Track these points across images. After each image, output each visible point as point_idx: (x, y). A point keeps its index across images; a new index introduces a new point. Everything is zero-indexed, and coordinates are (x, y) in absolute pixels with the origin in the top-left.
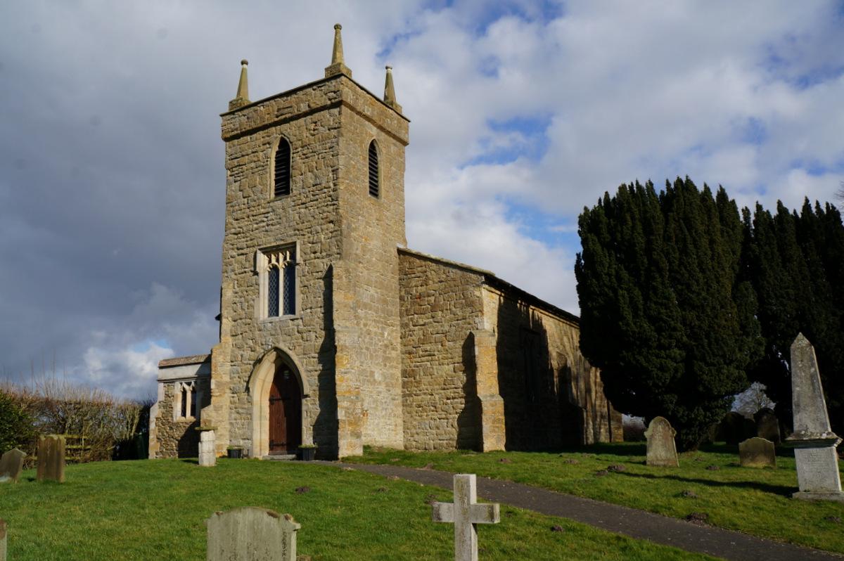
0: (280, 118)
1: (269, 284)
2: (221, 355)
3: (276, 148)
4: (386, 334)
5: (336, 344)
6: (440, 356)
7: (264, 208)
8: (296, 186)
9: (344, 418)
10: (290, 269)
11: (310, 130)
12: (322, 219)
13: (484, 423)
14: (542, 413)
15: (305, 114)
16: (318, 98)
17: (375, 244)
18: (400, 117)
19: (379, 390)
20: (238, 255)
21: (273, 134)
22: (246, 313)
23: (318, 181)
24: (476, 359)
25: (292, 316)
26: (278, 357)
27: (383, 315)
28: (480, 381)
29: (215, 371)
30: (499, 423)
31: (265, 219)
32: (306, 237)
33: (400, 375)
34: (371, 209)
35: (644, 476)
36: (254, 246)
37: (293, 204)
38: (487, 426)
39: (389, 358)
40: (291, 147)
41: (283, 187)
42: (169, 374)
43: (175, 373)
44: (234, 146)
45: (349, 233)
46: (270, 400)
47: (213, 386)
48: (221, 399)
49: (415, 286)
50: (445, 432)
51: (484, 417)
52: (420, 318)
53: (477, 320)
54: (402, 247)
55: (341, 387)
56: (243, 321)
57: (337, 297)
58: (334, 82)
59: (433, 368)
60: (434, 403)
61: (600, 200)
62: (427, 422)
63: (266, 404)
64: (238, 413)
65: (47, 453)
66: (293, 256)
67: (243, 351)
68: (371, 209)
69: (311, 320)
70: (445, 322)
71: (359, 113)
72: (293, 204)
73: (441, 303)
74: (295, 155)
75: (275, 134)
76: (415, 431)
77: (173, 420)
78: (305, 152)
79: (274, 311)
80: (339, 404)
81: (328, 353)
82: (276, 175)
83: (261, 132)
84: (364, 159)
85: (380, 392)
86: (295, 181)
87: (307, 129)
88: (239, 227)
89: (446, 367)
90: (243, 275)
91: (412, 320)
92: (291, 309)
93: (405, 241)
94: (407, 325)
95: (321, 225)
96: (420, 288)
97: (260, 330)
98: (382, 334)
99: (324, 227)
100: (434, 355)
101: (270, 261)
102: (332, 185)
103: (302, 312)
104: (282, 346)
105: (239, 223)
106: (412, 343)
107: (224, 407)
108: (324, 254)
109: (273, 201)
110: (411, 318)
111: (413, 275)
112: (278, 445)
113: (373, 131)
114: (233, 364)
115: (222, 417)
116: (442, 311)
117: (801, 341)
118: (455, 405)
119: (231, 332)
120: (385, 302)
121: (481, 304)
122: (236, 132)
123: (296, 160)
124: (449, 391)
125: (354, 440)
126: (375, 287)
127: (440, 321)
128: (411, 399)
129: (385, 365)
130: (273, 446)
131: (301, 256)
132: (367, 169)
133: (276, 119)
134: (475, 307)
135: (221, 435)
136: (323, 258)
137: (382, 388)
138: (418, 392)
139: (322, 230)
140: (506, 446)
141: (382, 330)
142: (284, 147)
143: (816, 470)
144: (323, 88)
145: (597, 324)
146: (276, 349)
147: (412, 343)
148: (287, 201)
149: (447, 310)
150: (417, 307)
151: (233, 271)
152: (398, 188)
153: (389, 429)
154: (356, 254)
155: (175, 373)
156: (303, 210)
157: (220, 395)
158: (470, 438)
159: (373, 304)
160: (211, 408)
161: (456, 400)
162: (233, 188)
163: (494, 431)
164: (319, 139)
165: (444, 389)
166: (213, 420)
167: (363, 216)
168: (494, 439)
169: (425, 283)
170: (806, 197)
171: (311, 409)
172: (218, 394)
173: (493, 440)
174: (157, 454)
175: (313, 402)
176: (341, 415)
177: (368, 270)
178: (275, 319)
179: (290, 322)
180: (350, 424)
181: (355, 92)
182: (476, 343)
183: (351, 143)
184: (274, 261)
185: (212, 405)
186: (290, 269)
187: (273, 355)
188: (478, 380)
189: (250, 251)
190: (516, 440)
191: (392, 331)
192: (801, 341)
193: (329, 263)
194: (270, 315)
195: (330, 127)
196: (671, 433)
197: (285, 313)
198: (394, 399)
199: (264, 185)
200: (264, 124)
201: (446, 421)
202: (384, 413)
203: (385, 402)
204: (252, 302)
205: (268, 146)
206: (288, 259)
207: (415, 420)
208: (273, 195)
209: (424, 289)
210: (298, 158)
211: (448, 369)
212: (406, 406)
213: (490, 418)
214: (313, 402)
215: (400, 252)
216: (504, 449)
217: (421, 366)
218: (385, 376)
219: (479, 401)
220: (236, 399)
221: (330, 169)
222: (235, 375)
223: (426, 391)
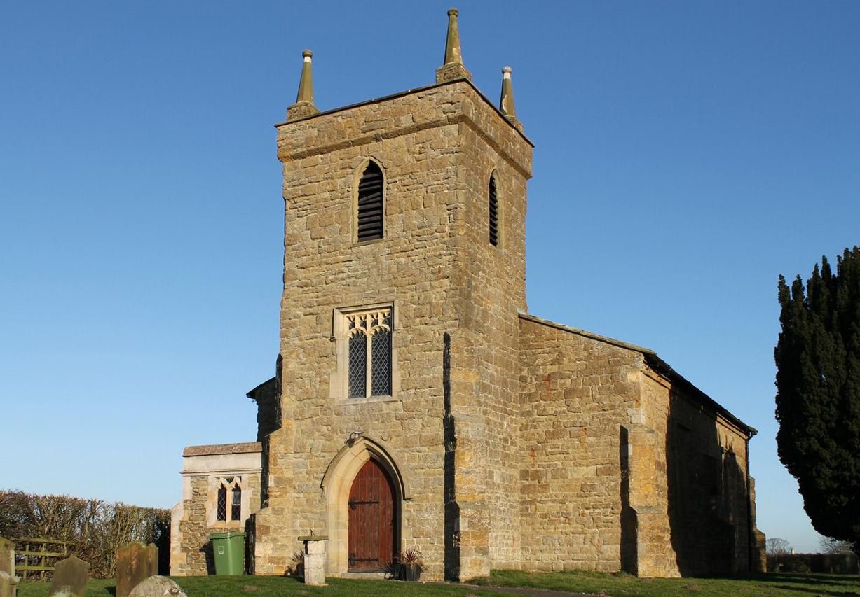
0: (368, 134)
1: (351, 355)
2: (281, 443)
4: (505, 423)
5: (456, 435)
6: (577, 455)
7: (343, 254)
8: (393, 226)
9: (467, 530)
11: (414, 153)
12: (432, 273)
13: (639, 541)
15: (408, 131)
17: (495, 308)
18: (523, 141)
19: (499, 495)
20: (305, 315)
21: (356, 155)
22: (317, 392)
23: (426, 223)
24: (630, 460)
25: (387, 398)
27: (502, 401)
28: (634, 489)
29: (275, 464)
30: (658, 541)
31: (346, 269)
32: (408, 295)
33: (518, 477)
34: (491, 262)
36: (328, 304)
37: (388, 251)
39: (508, 455)
40: (384, 174)
41: (371, 228)
42: (199, 464)
43: (208, 465)
44: (296, 168)
45: (469, 293)
46: (350, 503)
49: (543, 365)
51: (640, 534)
52: (549, 405)
53: (630, 412)
54: (523, 313)
56: (313, 400)
59: (565, 469)
60: (565, 514)
61: (816, 267)
62: (556, 537)
63: (345, 508)
64: (305, 518)
65: (131, 565)
67: (314, 439)
68: (491, 262)
69: (415, 403)
71: (480, 133)
72: (388, 251)
73: (581, 387)
74: (390, 186)
76: (538, 548)
77: (206, 525)
78: (405, 182)
79: (358, 388)
80: (461, 511)
83: (338, 152)
84: (485, 195)
85: (499, 498)
86: (391, 221)
87: (408, 151)
88: (306, 278)
89: (585, 468)
90: (313, 341)
91: (537, 407)
92: (384, 386)
93: (525, 307)
95: (431, 281)
96: (549, 367)
97: (339, 414)
98: (501, 424)
99: (436, 283)
100: (568, 453)
101: (353, 325)
102: (447, 229)
103: (402, 393)
105: (305, 273)
106: (536, 437)
107: (286, 511)
108: (435, 319)
109: (354, 246)
110: (536, 406)
111: (540, 350)
112: (361, 560)
113: (494, 157)
114: (298, 455)
115: (284, 523)
116: (581, 397)
118: (595, 517)
119: (295, 415)
120: (505, 384)
121: (638, 393)
122: (299, 150)
123: (391, 191)
124: (588, 499)
125: (478, 557)
126: (496, 364)
127: (577, 410)
128: (534, 507)
129: (504, 464)
131: (400, 320)
132: (487, 209)
133: (362, 136)
135: (282, 545)
136: (433, 324)
137: (500, 493)
138: (544, 499)
139: (432, 287)
141: (501, 419)
142: (373, 181)
144: (434, 97)
147: (536, 437)
149: (588, 396)
150: (545, 390)
151: (298, 334)
152: (519, 234)
153: (507, 544)
154: (476, 321)
155: (208, 465)
156: (403, 260)
157: (280, 496)
159: (493, 386)
161: (598, 511)
162: (296, 226)
163: (652, 551)
164: (428, 165)
165: (581, 496)
166: (271, 526)
167: (484, 272)
169: (558, 361)
170: (824, 256)
172: (278, 494)
173: (651, 563)
174: (182, 566)
175: (417, 507)
177: (488, 342)
178: (360, 401)
179: (385, 405)
180: (475, 537)
181: (477, 105)
182: (630, 440)
183: (472, 173)
185: (270, 508)
188: (630, 486)
189: (325, 311)
191: (512, 421)
193: (443, 332)
195: (443, 150)
197: (375, 393)
198: (512, 507)
199: (343, 223)
200: (343, 140)
201: (583, 536)
202: (502, 523)
203: (504, 510)
204: (326, 377)
205: (349, 171)
207: (538, 533)
208: (356, 238)
209: (555, 368)
210: (396, 190)
211: (585, 465)
212: (526, 516)
213: (647, 535)
214: (417, 507)
216: (675, 573)
217: (549, 466)
218: (503, 478)
220: (303, 500)
221: (445, 207)
222: (301, 470)
223: (554, 498)
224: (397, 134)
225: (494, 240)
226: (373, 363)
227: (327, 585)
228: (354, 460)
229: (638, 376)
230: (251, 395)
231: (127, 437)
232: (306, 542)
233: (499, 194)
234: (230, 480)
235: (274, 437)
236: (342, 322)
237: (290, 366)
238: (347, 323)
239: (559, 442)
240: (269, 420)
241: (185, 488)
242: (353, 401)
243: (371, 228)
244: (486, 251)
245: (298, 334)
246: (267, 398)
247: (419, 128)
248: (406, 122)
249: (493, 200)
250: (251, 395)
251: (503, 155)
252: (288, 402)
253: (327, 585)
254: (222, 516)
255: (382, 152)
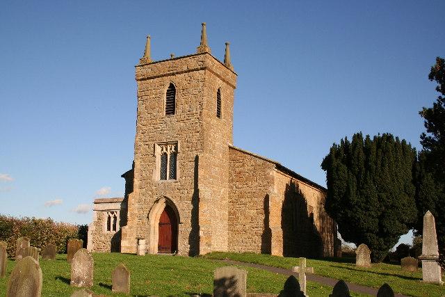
3: (167, 88)
8: (178, 110)
10: (174, 155)
14: (301, 236)
15: (186, 72)
16: (193, 63)
26: (166, 202)
35: (387, 274)
38: (273, 244)
41: (171, 109)
42: (100, 207)
47: (128, 215)
48: (132, 221)
50: (255, 246)
54: (231, 145)
55: (201, 218)
57: (201, 172)
58: (202, 56)
66: (176, 148)
70: (254, 185)
75: (167, 81)
79: (163, 177)
81: (196, 200)
82: (167, 103)
92: (174, 176)
94: (232, 188)
101: (162, 150)
104: (168, 196)
117: (429, 214)
123: (179, 97)
130: (160, 248)
134: (270, 181)
140: (284, 254)
142: (172, 90)
143: (431, 272)
145: (331, 197)
146: (165, 197)
148: (173, 118)
158: (266, 249)
160: (127, 227)
168: (277, 249)
171: (185, 229)
176: (201, 233)
178: (164, 181)
184: (165, 150)
186: (174, 155)
187: (164, 200)
190: (289, 251)
192: (429, 214)
194: (162, 178)
196: (369, 252)
197: (170, 178)
206: (173, 149)
211: (253, 211)
215: (230, 147)
216: (282, 256)
219: (270, 230)
224: (182, 72)
225: (219, 115)
226: (170, 166)
227: (419, 148)
228: (160, 208)
229: (274, 173)
230: (123, 176)
231: (66, 172)
232: (138, 240)
233: (222, 97)
234: (112, 213)
235: (130, 195)
236: (158, 149)
237: (137, 163)
238: (161, 149)
239: (243, 200)
240: (129, 188)
241: (95, 215)
242: (162, 181)
243: (171, 109)
244: (215, 121)
245: (141, 153)
246: (129, 176)
247: (189, 71)
248: (185, 68)
249: (219, 99)
250: (123, 176)
251: (224, 80)
252: (136, 182)
253: (419, 148)
254: (109, 229)
255: (178, 80)
